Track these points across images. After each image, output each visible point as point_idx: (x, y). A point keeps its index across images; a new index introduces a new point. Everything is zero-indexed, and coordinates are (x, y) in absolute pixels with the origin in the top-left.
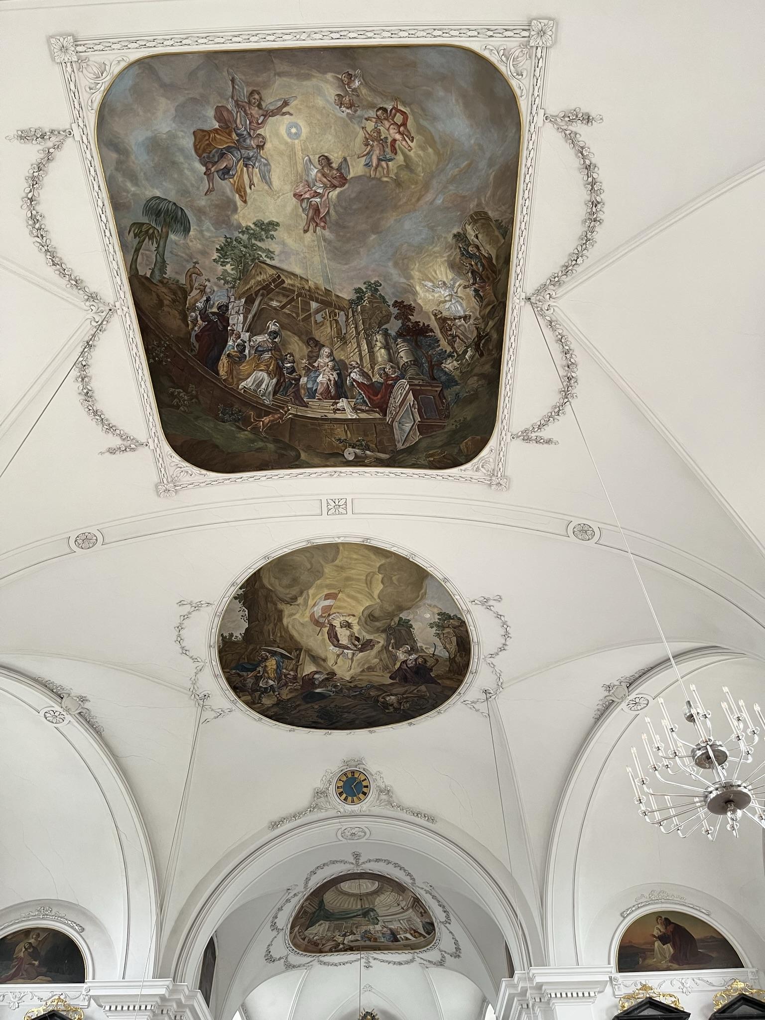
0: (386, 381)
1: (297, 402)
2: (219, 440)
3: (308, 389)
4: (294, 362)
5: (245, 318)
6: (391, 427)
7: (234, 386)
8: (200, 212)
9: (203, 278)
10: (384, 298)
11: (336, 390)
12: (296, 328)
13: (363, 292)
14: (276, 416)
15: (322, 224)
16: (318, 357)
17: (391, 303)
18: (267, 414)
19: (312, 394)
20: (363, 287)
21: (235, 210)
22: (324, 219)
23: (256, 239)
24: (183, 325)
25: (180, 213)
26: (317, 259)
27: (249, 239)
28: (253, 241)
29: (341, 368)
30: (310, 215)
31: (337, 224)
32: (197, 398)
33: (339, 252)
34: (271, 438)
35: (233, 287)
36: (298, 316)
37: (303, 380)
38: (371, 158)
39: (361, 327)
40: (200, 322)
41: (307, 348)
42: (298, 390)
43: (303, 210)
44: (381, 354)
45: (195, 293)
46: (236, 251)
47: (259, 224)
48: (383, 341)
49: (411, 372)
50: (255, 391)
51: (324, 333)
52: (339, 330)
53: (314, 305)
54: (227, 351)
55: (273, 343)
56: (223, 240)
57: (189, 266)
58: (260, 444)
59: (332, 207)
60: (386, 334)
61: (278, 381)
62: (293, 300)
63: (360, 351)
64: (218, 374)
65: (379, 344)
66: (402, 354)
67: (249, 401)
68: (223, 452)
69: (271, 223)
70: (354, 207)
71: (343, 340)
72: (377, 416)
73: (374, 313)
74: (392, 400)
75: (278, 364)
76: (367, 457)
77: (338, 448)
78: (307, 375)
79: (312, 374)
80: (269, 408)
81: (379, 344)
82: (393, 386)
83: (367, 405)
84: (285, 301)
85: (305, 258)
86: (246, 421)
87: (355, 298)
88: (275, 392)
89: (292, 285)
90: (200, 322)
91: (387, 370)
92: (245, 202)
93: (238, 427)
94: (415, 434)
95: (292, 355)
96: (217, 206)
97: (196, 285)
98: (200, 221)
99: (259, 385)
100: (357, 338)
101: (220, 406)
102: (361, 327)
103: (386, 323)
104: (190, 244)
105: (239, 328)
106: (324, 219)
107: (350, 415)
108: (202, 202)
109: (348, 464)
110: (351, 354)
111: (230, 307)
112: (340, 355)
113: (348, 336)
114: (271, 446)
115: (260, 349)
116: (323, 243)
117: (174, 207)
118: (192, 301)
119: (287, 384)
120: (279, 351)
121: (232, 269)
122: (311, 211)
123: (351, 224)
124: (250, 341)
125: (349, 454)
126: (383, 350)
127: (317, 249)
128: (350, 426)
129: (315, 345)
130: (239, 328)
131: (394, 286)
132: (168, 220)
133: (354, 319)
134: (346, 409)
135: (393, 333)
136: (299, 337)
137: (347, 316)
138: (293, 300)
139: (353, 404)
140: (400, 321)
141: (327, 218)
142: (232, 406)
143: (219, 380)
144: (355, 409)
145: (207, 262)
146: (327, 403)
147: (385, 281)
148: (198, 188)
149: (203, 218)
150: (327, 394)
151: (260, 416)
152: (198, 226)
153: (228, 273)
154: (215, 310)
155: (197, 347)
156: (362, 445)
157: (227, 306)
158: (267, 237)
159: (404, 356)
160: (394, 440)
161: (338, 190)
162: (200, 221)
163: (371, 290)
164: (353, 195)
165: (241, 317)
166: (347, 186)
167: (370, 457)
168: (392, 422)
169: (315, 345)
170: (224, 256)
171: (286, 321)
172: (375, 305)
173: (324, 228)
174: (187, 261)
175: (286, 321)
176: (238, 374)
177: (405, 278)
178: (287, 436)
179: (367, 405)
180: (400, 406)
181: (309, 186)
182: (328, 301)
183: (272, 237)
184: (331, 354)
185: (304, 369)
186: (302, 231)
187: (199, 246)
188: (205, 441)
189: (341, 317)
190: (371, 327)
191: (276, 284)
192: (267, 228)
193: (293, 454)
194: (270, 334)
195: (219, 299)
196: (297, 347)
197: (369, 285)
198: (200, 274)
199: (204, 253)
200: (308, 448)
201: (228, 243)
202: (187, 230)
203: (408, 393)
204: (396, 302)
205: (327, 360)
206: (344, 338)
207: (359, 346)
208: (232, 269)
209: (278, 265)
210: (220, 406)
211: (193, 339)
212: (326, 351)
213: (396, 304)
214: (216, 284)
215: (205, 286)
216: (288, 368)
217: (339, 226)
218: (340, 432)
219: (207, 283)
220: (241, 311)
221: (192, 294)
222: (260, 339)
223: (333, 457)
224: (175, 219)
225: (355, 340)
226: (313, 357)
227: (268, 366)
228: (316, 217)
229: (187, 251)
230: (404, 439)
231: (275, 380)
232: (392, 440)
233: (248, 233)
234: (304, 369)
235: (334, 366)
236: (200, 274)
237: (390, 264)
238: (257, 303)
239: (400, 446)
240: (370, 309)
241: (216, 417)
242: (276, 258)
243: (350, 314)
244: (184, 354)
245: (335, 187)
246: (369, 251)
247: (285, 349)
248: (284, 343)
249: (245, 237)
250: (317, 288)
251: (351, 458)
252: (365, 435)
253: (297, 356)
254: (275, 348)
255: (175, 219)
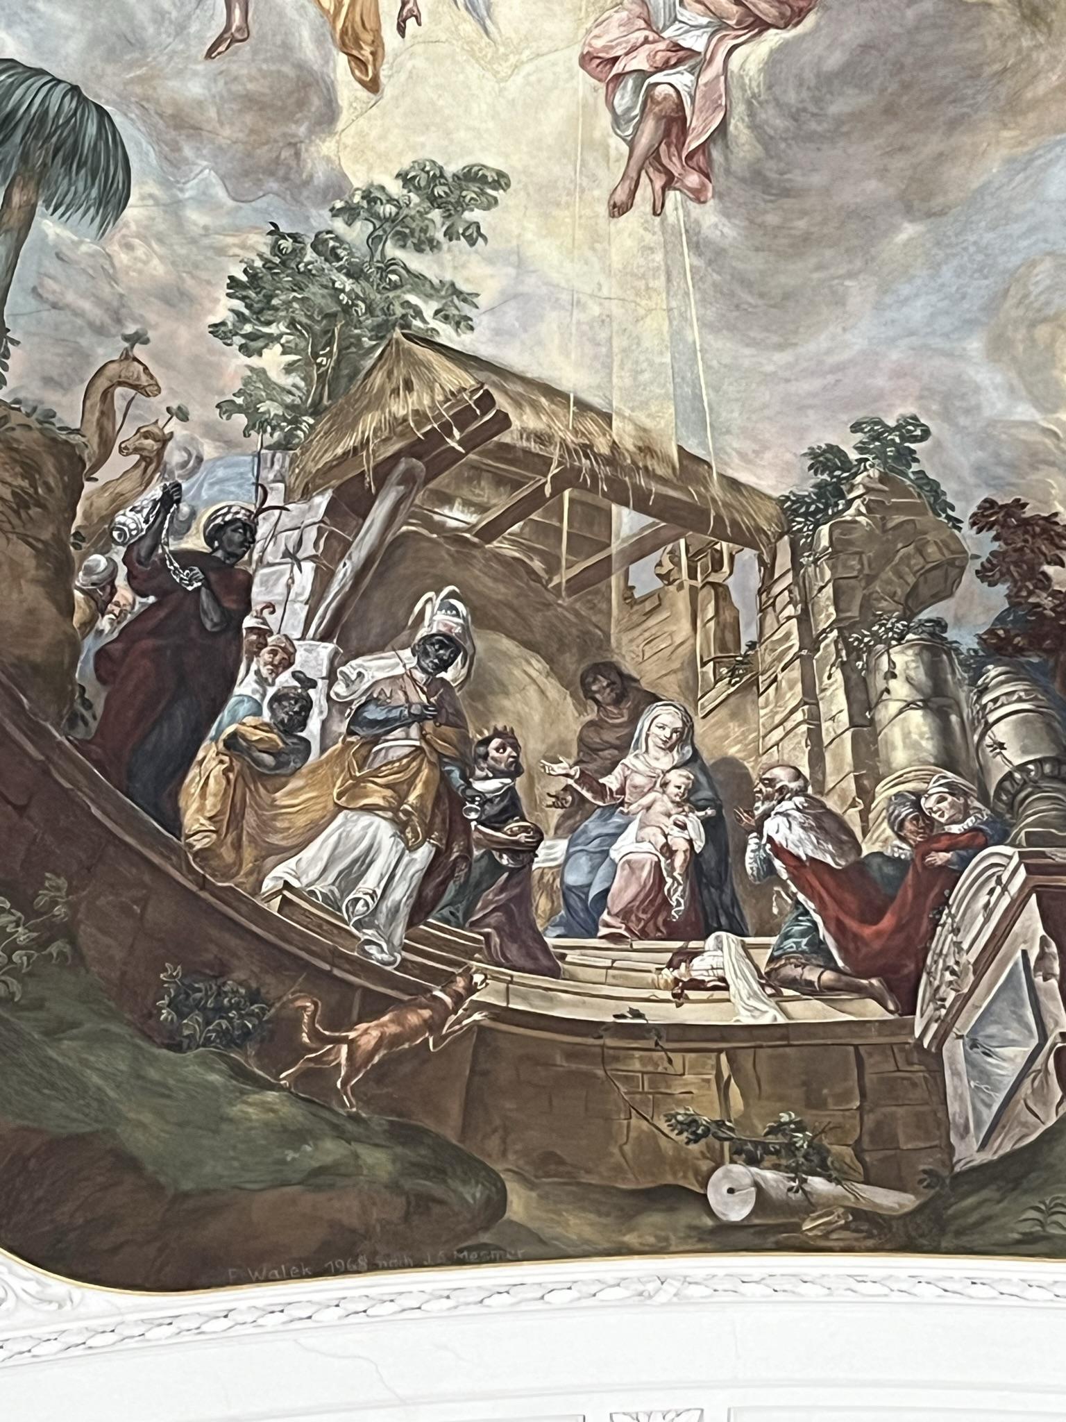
0: (922, 850)
1: (514, 952)
2: (145, 1131)
3: (567, 890)
4: (515, 770)
5: (323, 579)
6: (933, 1060)
7: (240, 882)
8: (180, 124)
9: (160, 403)
10: (933, 489)
11: (695, 897)
12: (537, 620)
13: (846, 464)
14: (413, 1019)
15: (693, 179)
16: (623, 747)
17: (965, 510)
18: (374, 1007)
19: (583, 914)
20: (849, 446)
21: (328, 117)
22: (700, 160)
23: (402, 240)
24: (48, 610)
25: (92, 129)
26: (654, 328)
27: (374, 240)
28: (392, 250)
29: (723, 796)
30: (644, 141)
31: (756, 178)
32: (73, 942)
33: (753, 300)
34: (379, 1122)
35: (285, 445)
36: (553, 568)
37: (551, 852)
38: (965, 862)
39: (826, 614)
40: (124, 593)
41: (581, 708)
42: (524, 899)
43: (617, 120)
44: (908, 734)
45: (117, 465)
46: (314, 291)
47: (426, 181)
48: (920, 675)
49: (1036, 812)
50: (332, 903)
51: (661, 644)
52: (728, 630)
53: (627, 522)
54: (225, 724)
55: (434, 685)
56: (262, 243)
57: (107, 352)
58: (331, 1150)
59: (740, 109)
60: (935, 646)
61: (439, 855)
62: (536, 500)
63: (814, 720)
64: (174, 824)
65: (900, 689)
66: (1001, 732)
67: (310, 956)
68: (156, 1188)
69: (472, 176)
70: (836, 108)
71: (742, 669)
72: (873, 1010)
73: (886, 557)
74: (943, 939)
75: (445, 778)
76: (810, 1205)
77: (681, 1162)
78: (569, 828)
79: (593, 826)
80: (388, 979)
81: (900, 689)
82: (951, 875)
83: (830, 964)
84: (501, 503)
85: (605, 320)
86: (278, 1042)
87: (807, 489)
88: (420, 908)
89: (541, 438)
90: (124, 593)
91: (926, 804)
92: (373, 86)
93: (239, 1072)
94: (1041, 1094)
95: (509, 739)
96: (250, 102)
97: (127, 433)
98: (173, 162)
99: (351, 877)
100: (806, 662)
101: (171, 973)
102: (826, 614)
103: (937, 598)
104: (123, 258)
105: (291, 622)
106: (700, 160)
107: (748, 1007)
108: (194, 85)
109: (725, 1238)
110: (768, 736)
111: (263, 529)
112: (722, 739)
113: (765, 656)
114: (378, 1161)
115: (373, 713)
116: (689, 260)
117: (70, 104)
118: (103, 502)
119: (476, 866)
120: (457, 721)
121: (289, 369)
122: (649, 125)
123: (817, 180)
124: (331, 678)
125: (731, 1194)
126: (916, 718)
127: (660, 283)
128: (746, 1061)
129: (616, 695)
130: (291, 622)
131: (983, 439)
132: (38, 158)
133: (801, 583)
134: (733, 984)
135: (966, 639)
136: (549, 660)
137: (768, 569)
138: (536, 500)
139: (762, 957)
140: (1002, 589)
141: (716, 154)
142: (222, 971)
143: (177, 854)
144: (773, 981)
145: (184, 334)
146: (650, 957)
147: (946, 415)
148: (181, 29)
149: (188, 151)
150: (651, 916)
151: (339, 1019)
152: (165, 184)
153: (268, 383)
154: (195, 542)
155: (99, 709)
156: (791, 1148)
157: (249, 528)
158: (450, 235)
159: (1010, 743)
160: (944, 1124)
161: (773, 38)
162: (173, 162)
163: (881, 455)
164: (835, 60)
165: (305, 576)
166: (810, 21)
167: (828, 1205)
168: (940, 1038)
169: (616, 695)
170: (262, 310)
171: (500, 591)
172: (898, 519)
173: (697, 196)
174: (100, 331)
175: (500, 591)
176: (265, 826)
177: (1038, 403)
178: (455, 1107)
179: (830, 964)
180: (980, 967)
181: (649, 24)
182: (691, 508)
183: (474, 235)
184: (685, 735)
185: (558, 801)
186: (603, 210)
187: (158, 268)
188: (80, 1140)
189: (742, 576)
190: (869, 613)
191: (471, 434)
192: (453, 195)
193: (474, 1193)
194: (421, 651)
195: (216, 494)
196: (537, 708)
197: (874, 433)
198: (146, 389)
199: (176, 299)
200: (546, 1168)
201: (284, 257)
202: (113, 200)
203: (1018, 905)
204: (989, 504)
205: (665, 761)
206: (747, 661)
207: (810, 696)
208: (289, 369)
209: (485, 351)
210: (171, 973)
211: (84, 671)
212: (665, 718)
213: (988, 514)
214: (210, 431)
215: (164, 440)
216: (485, 801)
217: (765, 184)
218: (697, 1089)
219: (174, 426)
220: (308, 550)
221: (103, 475)
222: (375, 668)
223: (656, 1209)
224: (69, 153)
225: (795, 672)
226: (600, 750)
227: (399, 791)
228: (669, 147)
229: (106, 290)
230: (988, 1116)
231: (424, 854)
232: (935, 1122)
233: (373, 215)
234: (558, 801)
235: (693, 789)
236: (146, 389)
237: (975, 345)
238: (379, 512)
239: (969, 1153)
240: (870, 536)
241: (147, 1026)
242: (483, 322)
243: (784, 560)
244: (38, 734)
245: (759, 25)
246: (884, 289)
247: (483, 717)
248: (483, 687)
249: (357, 233)
250: (647, 450)
251: (737, 1211)
252: (814, 1102)
253: (532, 746)
254: (442, 710)
255: (69, 153)
